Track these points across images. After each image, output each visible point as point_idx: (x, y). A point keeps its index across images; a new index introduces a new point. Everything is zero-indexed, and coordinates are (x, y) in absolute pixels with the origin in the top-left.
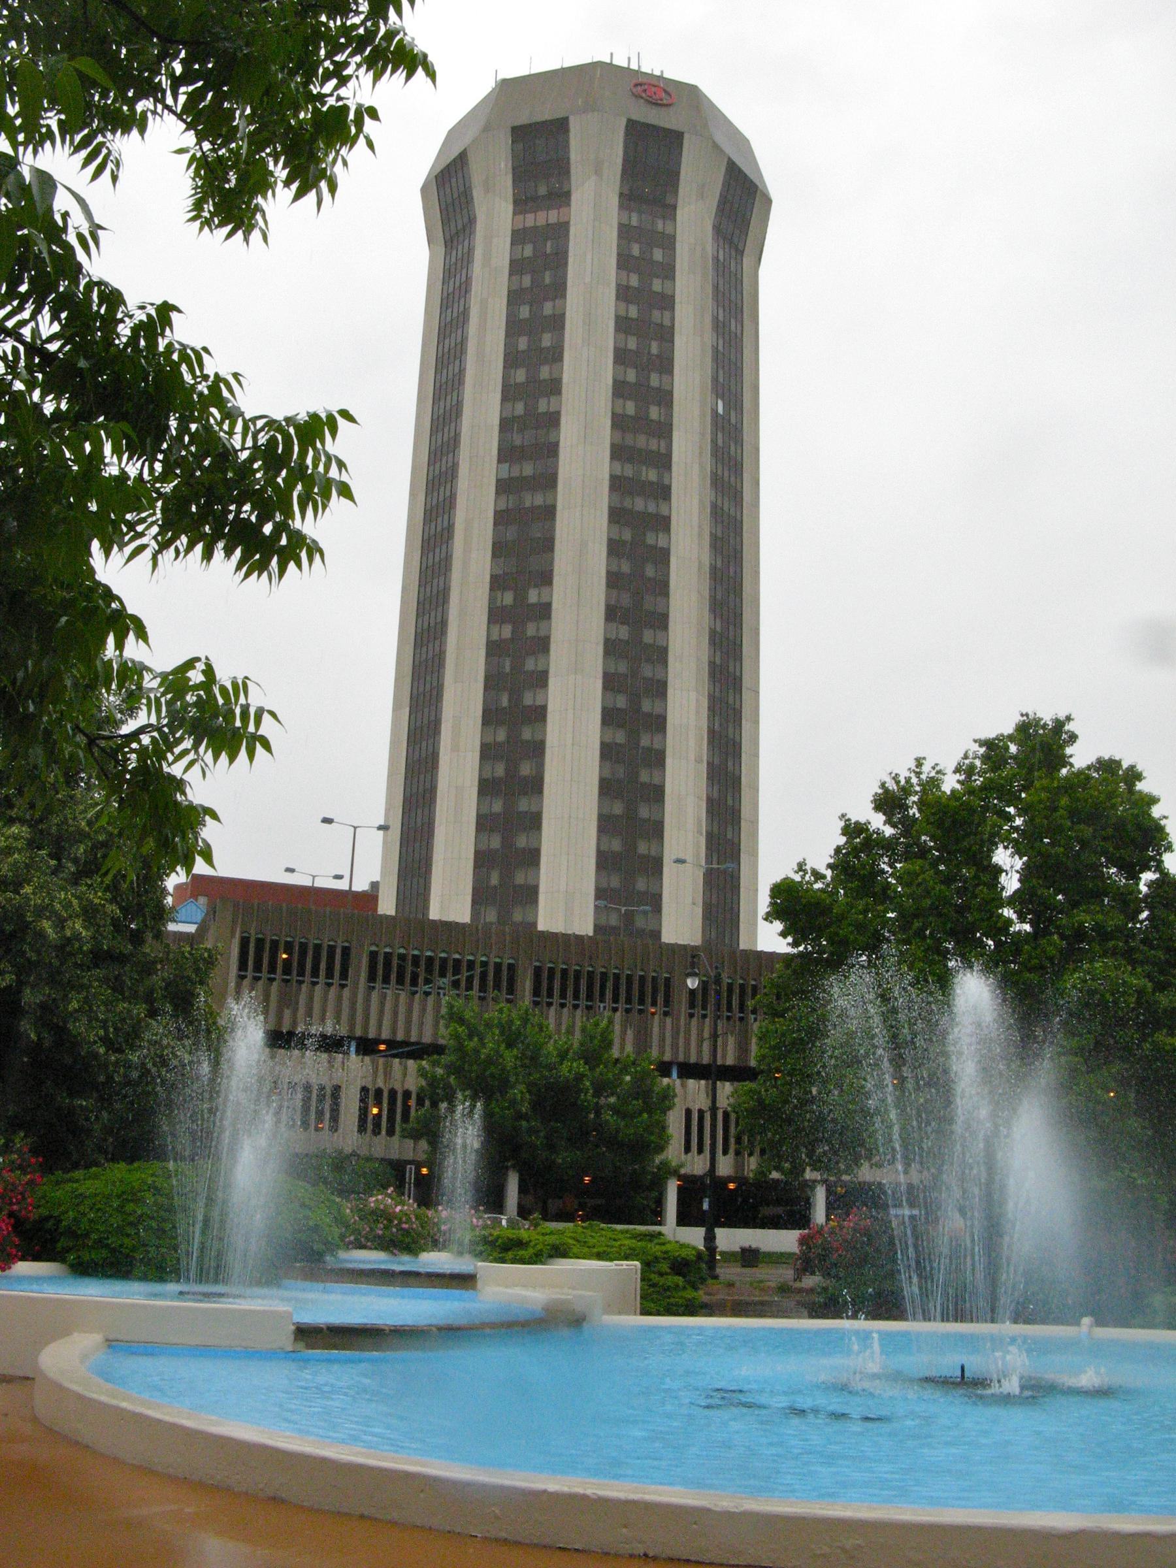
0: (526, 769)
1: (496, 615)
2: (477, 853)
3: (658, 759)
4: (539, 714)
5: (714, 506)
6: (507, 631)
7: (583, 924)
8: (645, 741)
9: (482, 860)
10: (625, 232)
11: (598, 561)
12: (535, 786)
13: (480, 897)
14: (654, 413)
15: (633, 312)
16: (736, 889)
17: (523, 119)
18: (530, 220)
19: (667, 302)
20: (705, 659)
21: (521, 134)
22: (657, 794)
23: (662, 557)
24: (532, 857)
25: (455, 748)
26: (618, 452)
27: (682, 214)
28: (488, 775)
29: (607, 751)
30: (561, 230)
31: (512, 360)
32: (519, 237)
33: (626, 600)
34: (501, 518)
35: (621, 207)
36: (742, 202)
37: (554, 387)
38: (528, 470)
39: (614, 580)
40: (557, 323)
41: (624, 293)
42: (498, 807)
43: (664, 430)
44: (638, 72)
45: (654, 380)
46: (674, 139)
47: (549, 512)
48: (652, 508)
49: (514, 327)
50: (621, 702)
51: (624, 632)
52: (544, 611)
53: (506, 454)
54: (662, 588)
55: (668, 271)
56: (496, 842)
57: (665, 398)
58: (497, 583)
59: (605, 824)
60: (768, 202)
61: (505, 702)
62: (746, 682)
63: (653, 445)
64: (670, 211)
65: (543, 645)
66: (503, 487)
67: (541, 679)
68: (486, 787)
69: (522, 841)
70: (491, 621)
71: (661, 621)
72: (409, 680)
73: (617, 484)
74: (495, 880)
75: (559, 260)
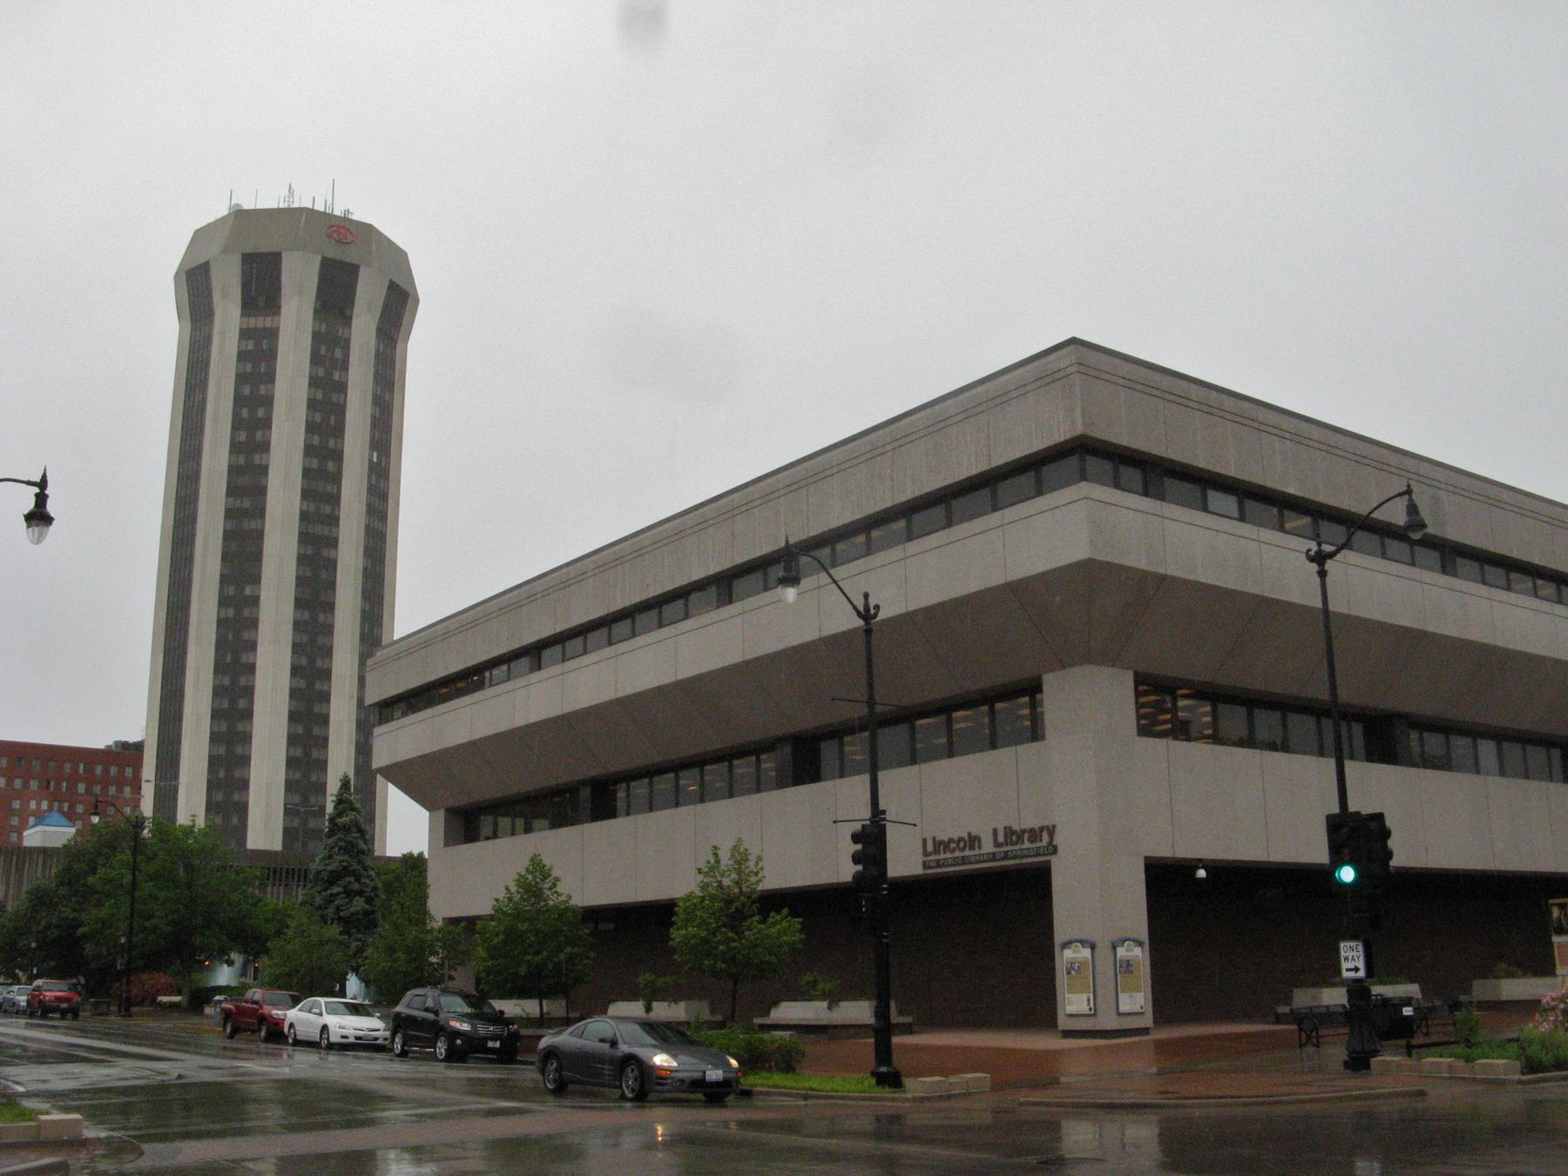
0: (242, 704)
1: (223, 601)
2: (211, 757)
3: (325, 697)
4: (251, 669)
5: (367, 526)
6: (231, 612)
7: (276, 843)
8: (314, 778)
9: (214, 762)
10: (316, 336)
11: (302, 392)
12: (248, 714)
13: (211, 807)
14: (331, 466)
15: (319, 395)
16: (382, 583)
17: (250, 249)
18: (253, 322)
19: (342, 387)
20: (361, 566)
21: (248, 259)
22: (324, 720)
23: (332, 565)
24: (245, 761)
25: (196, 687)
26: (306, 494)
27: (355, 323)
28: (223, 615)
29: (294, 693)
30: (273, 334)
31: (237, 424)
32: (245, 334)
33: (304, 661)
34: (227, 536)
35: (315, 319)
36: (399, 303)
37: (265, 447)
38: (246, 503)
39: (301, 582)
40: (268, 401)
41: (314, 382)
42: (224, 727)
43: (336, 478)
44: (330, 216)
45: (331, 443)
46: (349, 255)
47: (260, 535)
48: (326, 532)
49: (239, 401)
50: (304, 661)
51: (306, 615)
52: (255, 601)
53: (232, 491)
54: (331, 585)
55: (345, 365)
56: (222, 750)
57: (338, 456)
58: (225, 580)
59: (292, 740)
60: (417, 301)
61: (229, 659)
62: (403, 328)
63: (329, 488)
64: (348, 321)
65: (254, 623)
66: (230, 513)
67: (253, 646)
68: (216, 715)
69: (243, 681)
70: (220, 604)
71: (330, 608)
72: (178, 441)
73: (304, 516)
74: (222, 774)
75: (271, 356)
